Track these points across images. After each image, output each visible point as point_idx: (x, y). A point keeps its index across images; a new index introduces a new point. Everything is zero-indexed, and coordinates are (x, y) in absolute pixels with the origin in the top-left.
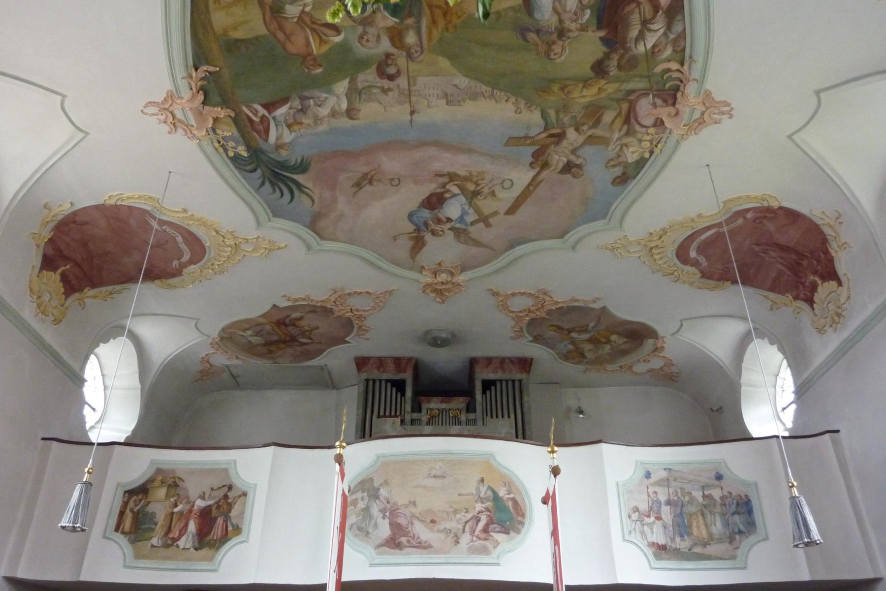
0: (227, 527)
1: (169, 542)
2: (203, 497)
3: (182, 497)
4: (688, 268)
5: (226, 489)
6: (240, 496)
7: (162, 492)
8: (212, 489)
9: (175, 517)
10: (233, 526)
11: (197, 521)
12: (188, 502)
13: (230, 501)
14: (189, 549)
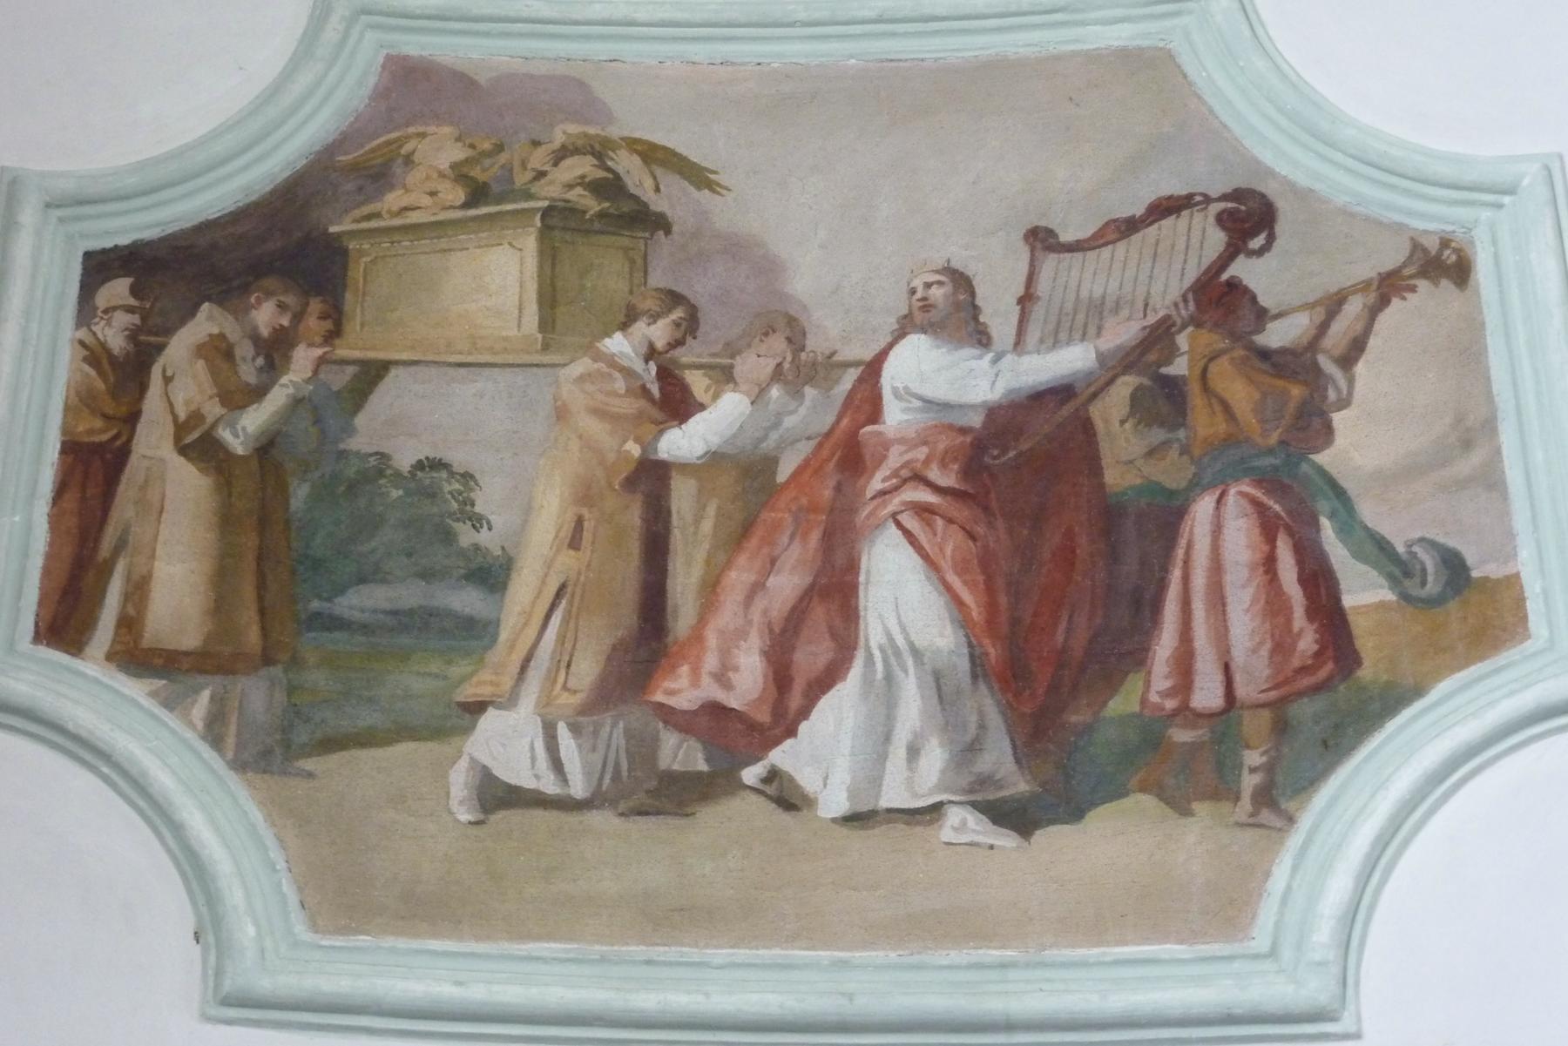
0: (1319, 582)
1: (681, 754)
2: (954, 312)
3: (717, 326)
4: (1280, 778)
5: (1203, 238)
6: (1388, 287)
7: (497, 278)
8: (1041, 240)
9: (694, 524)
10: (1379, 551)
11: (951, 544)
12: (803, 369)
13: (1276, 336)
14: (936, 809)
